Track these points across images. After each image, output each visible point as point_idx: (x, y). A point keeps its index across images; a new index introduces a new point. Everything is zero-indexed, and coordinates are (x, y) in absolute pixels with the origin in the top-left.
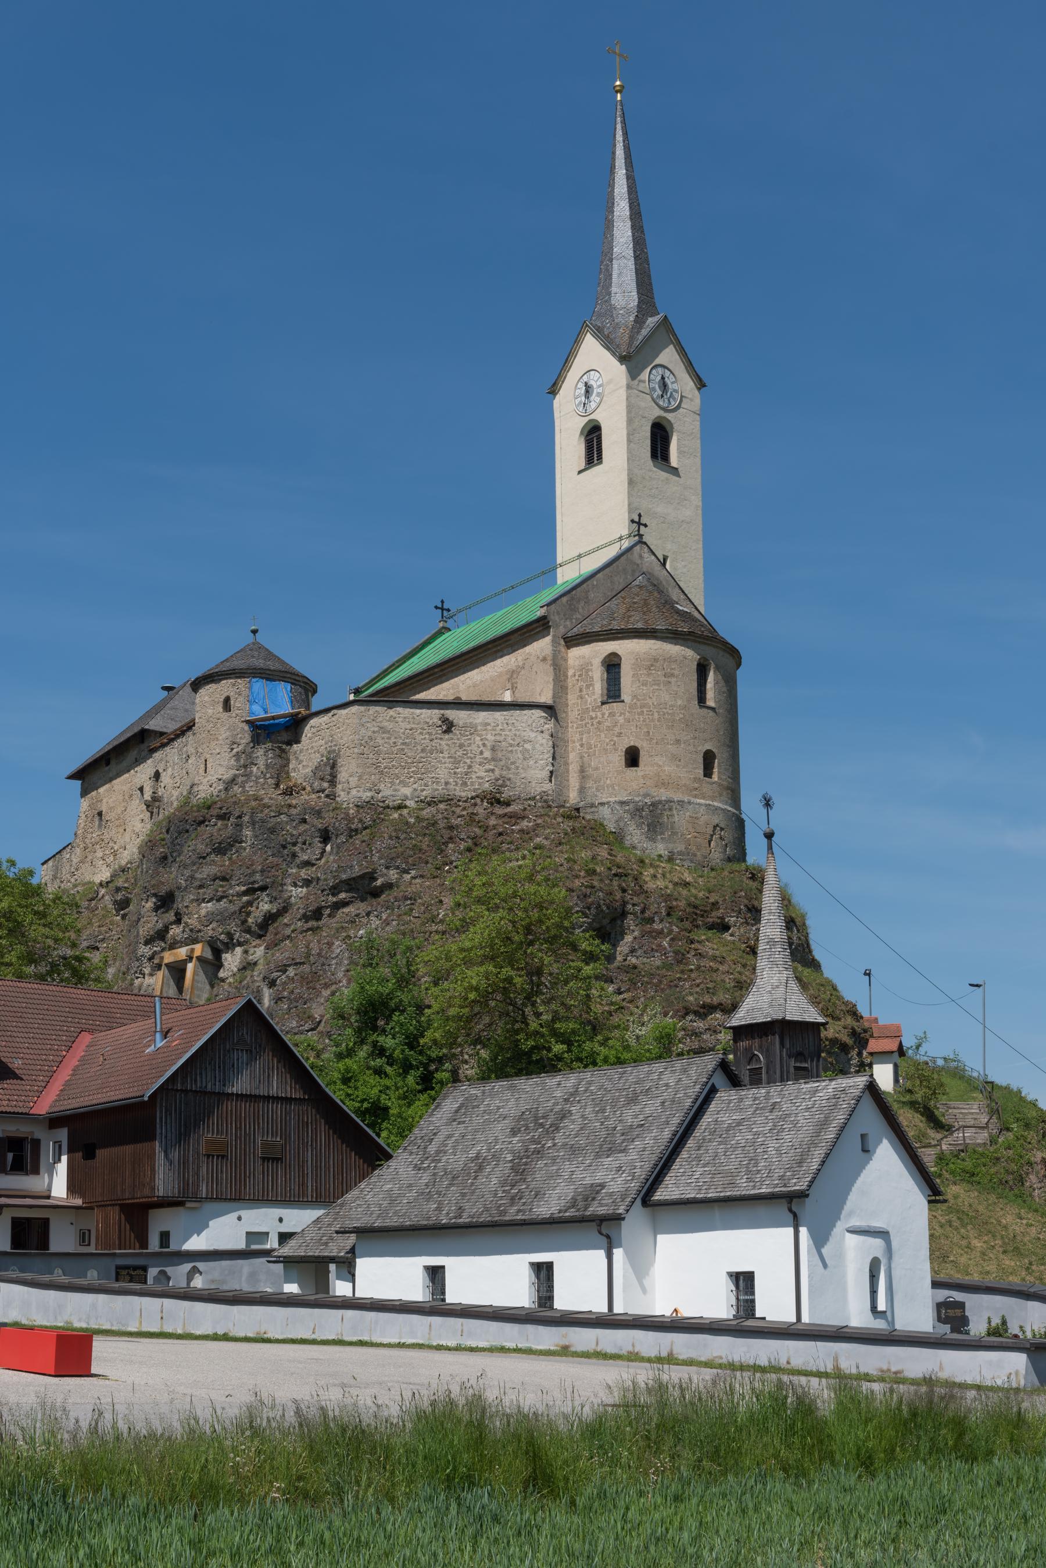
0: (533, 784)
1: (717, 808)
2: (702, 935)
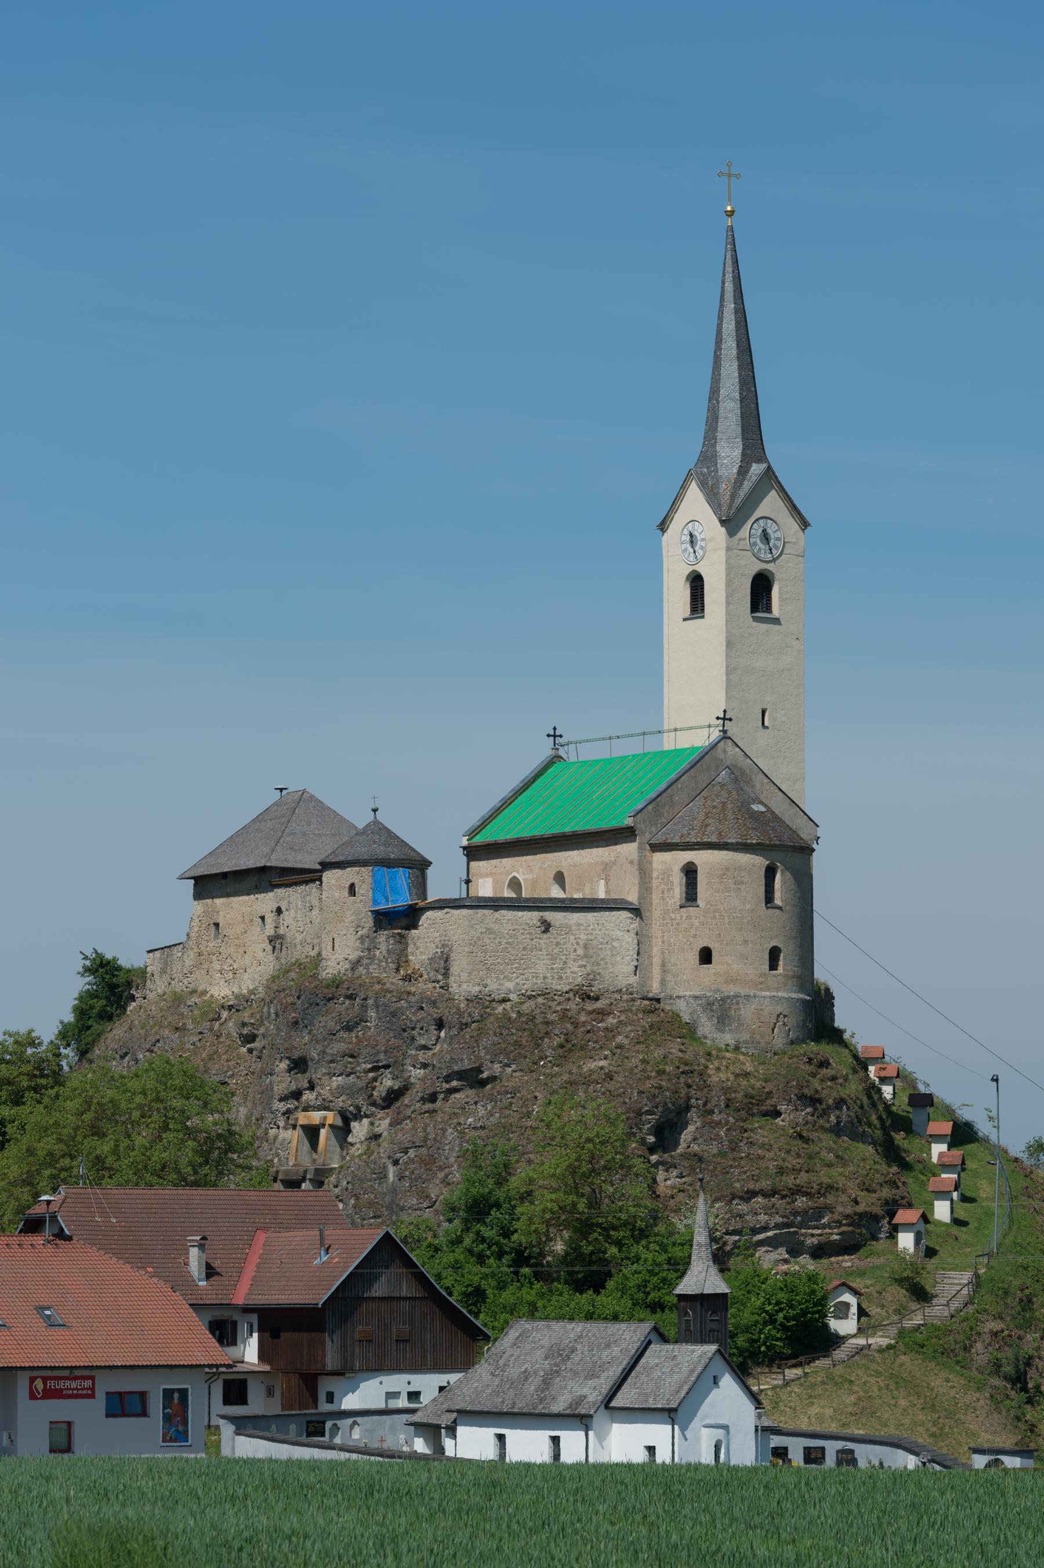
0: (620, 978)
1: (780, 999)
2: (756, 1123)
